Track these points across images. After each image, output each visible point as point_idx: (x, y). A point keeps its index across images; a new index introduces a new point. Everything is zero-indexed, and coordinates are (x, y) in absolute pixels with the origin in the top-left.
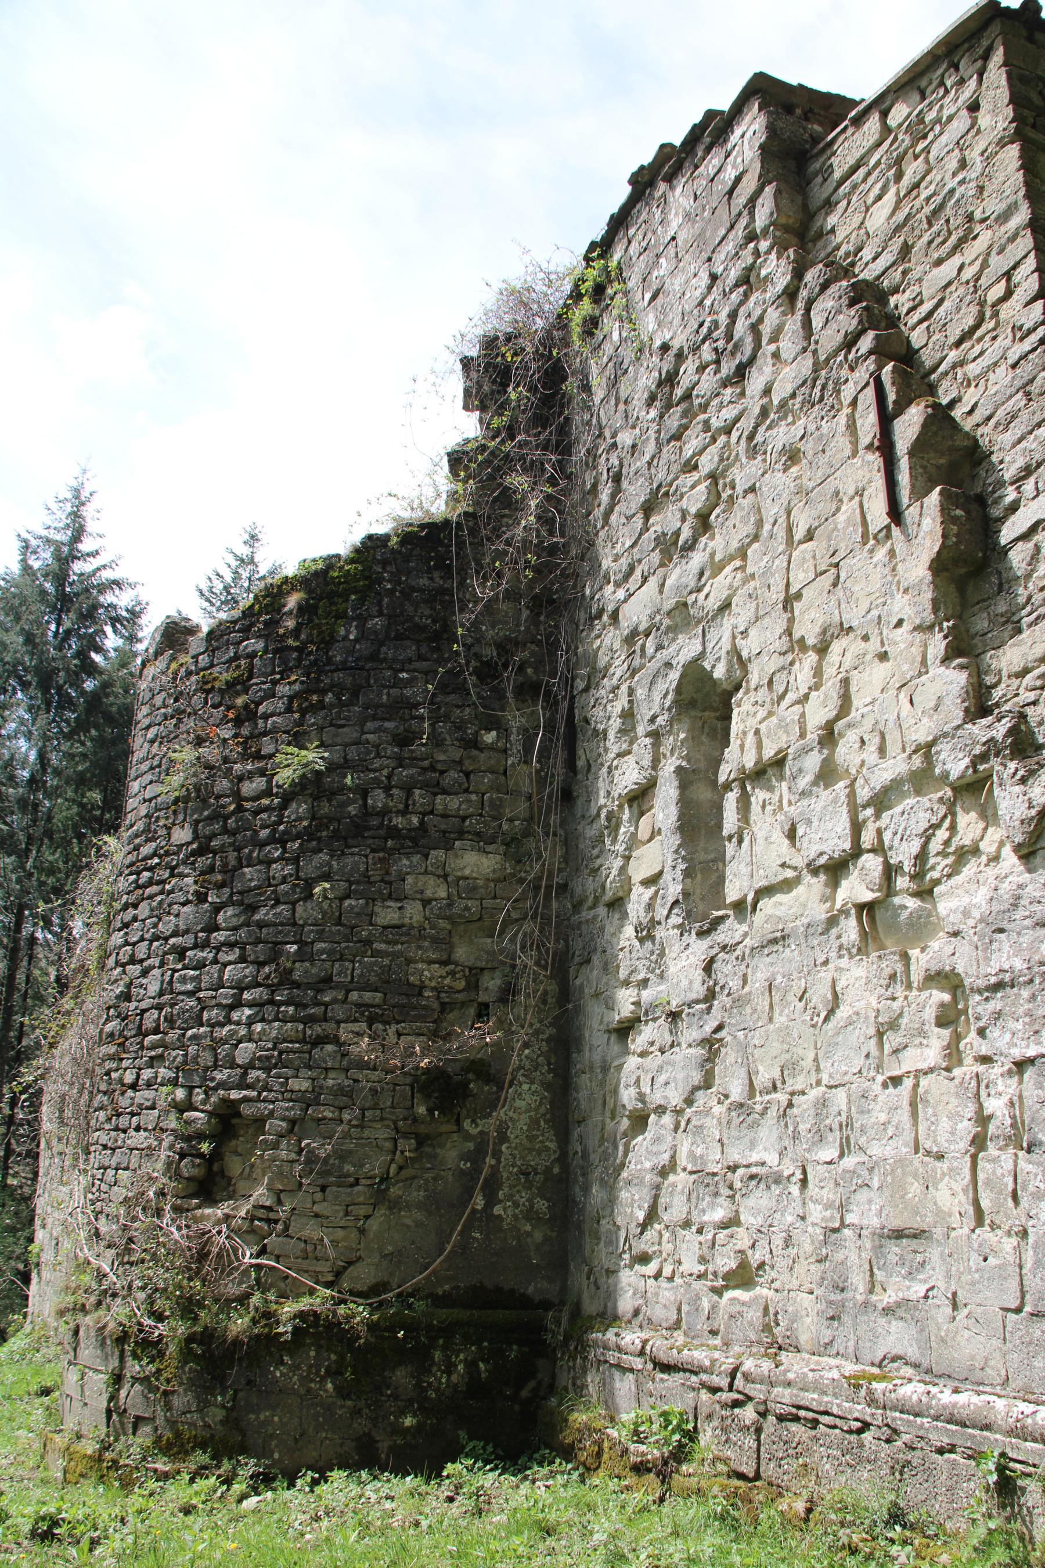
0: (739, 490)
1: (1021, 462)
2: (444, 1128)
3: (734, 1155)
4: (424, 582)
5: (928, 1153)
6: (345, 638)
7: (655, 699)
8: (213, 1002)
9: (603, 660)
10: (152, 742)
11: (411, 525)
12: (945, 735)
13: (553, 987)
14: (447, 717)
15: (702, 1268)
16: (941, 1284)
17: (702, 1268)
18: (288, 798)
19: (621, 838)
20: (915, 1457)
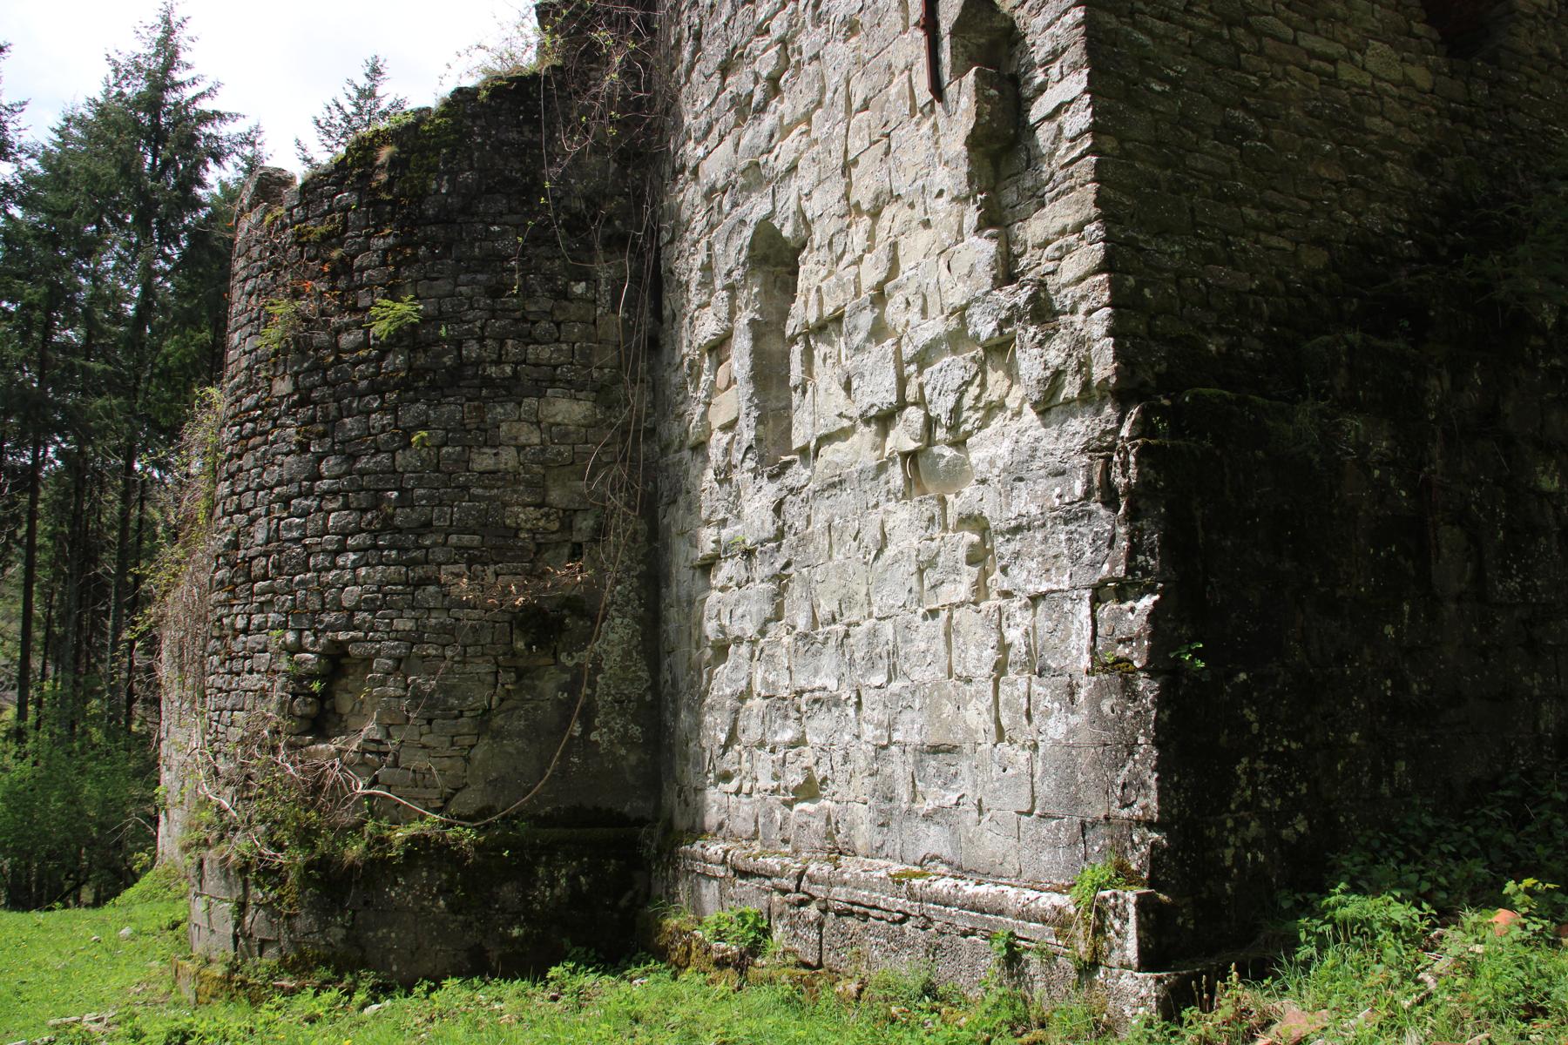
0: (806, 56)
1: (1048, 47)
2: (542, 661)
3: (801, 681)
4: (513, 135)
5: (959, 678)
6: (438, 191)
7: (732, 254)
8: (319, 548)
9: (685, 215)
10: (250, 294)
11: (501, 78)
12: (976, 300)
13: (643, 526)
15: (775, 784)
16: (969, 793)
17: (775, 784)
18: (384, 350)
19: (702, 385)
20: (945, 941)
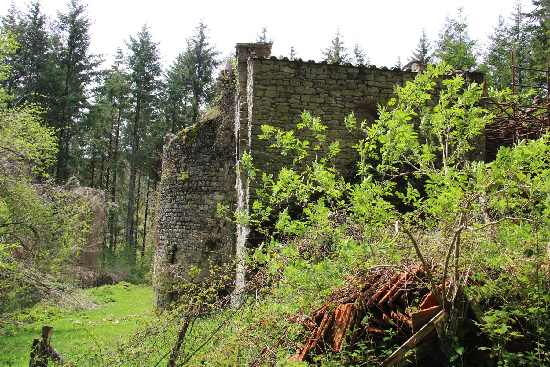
4: (209, 134)
14: (213, 165)
18: (184, 182)
